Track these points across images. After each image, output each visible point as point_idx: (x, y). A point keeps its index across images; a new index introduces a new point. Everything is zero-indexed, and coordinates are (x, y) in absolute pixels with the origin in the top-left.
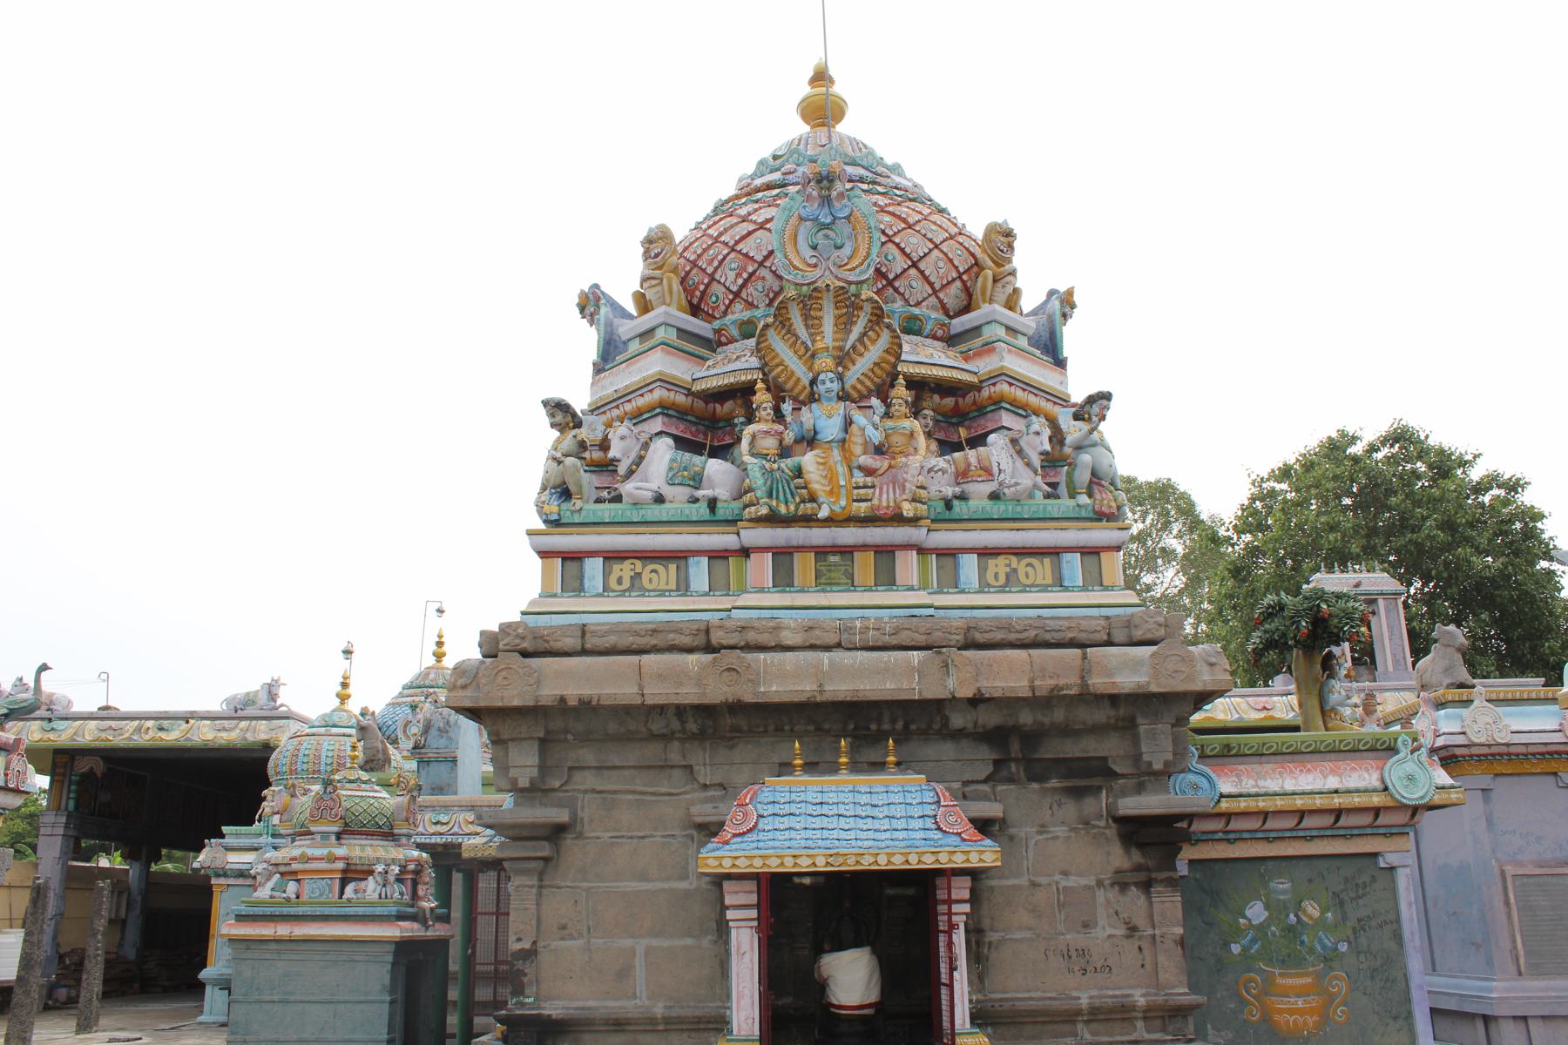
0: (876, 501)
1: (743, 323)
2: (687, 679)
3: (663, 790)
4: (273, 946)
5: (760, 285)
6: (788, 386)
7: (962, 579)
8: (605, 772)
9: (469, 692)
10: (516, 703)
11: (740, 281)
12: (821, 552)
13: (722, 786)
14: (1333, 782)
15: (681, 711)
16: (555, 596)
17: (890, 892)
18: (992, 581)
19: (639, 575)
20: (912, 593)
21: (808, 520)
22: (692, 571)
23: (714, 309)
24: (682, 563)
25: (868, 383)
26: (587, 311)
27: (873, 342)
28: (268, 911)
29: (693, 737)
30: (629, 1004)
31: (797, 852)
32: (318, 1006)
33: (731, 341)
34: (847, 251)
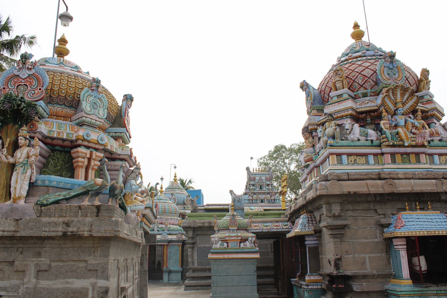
0: (417, 141)
1: (364, 93)
2: (377, 187)
3: (369, 216)
4: (223, 260)
5: (369, 84)
6: (389, 111)
7: (435, 161)
8: (354, 211)
9: (325, 191)
10: (338, 193)
11: (363, 82)
12: (402, 154)
13: (384, 214)
14: (265, 219)
15: (375, 195)
16: (335, 165)
17: (431, 241)
18: (442, 162)
19: (356, 160)
20: (424, 165)
21: (403, 146)
22: (369, 158)
23: (354, 89)
24: (366, 157)
25: (409, 111)
26: (304, 88)
27: (411, 100)
28: (221, 251)
29: (378, 202)
30: (366, 271)
31: (419, 231)
32: (237, 276)
33: (359, 98)
34: (397, 75)
